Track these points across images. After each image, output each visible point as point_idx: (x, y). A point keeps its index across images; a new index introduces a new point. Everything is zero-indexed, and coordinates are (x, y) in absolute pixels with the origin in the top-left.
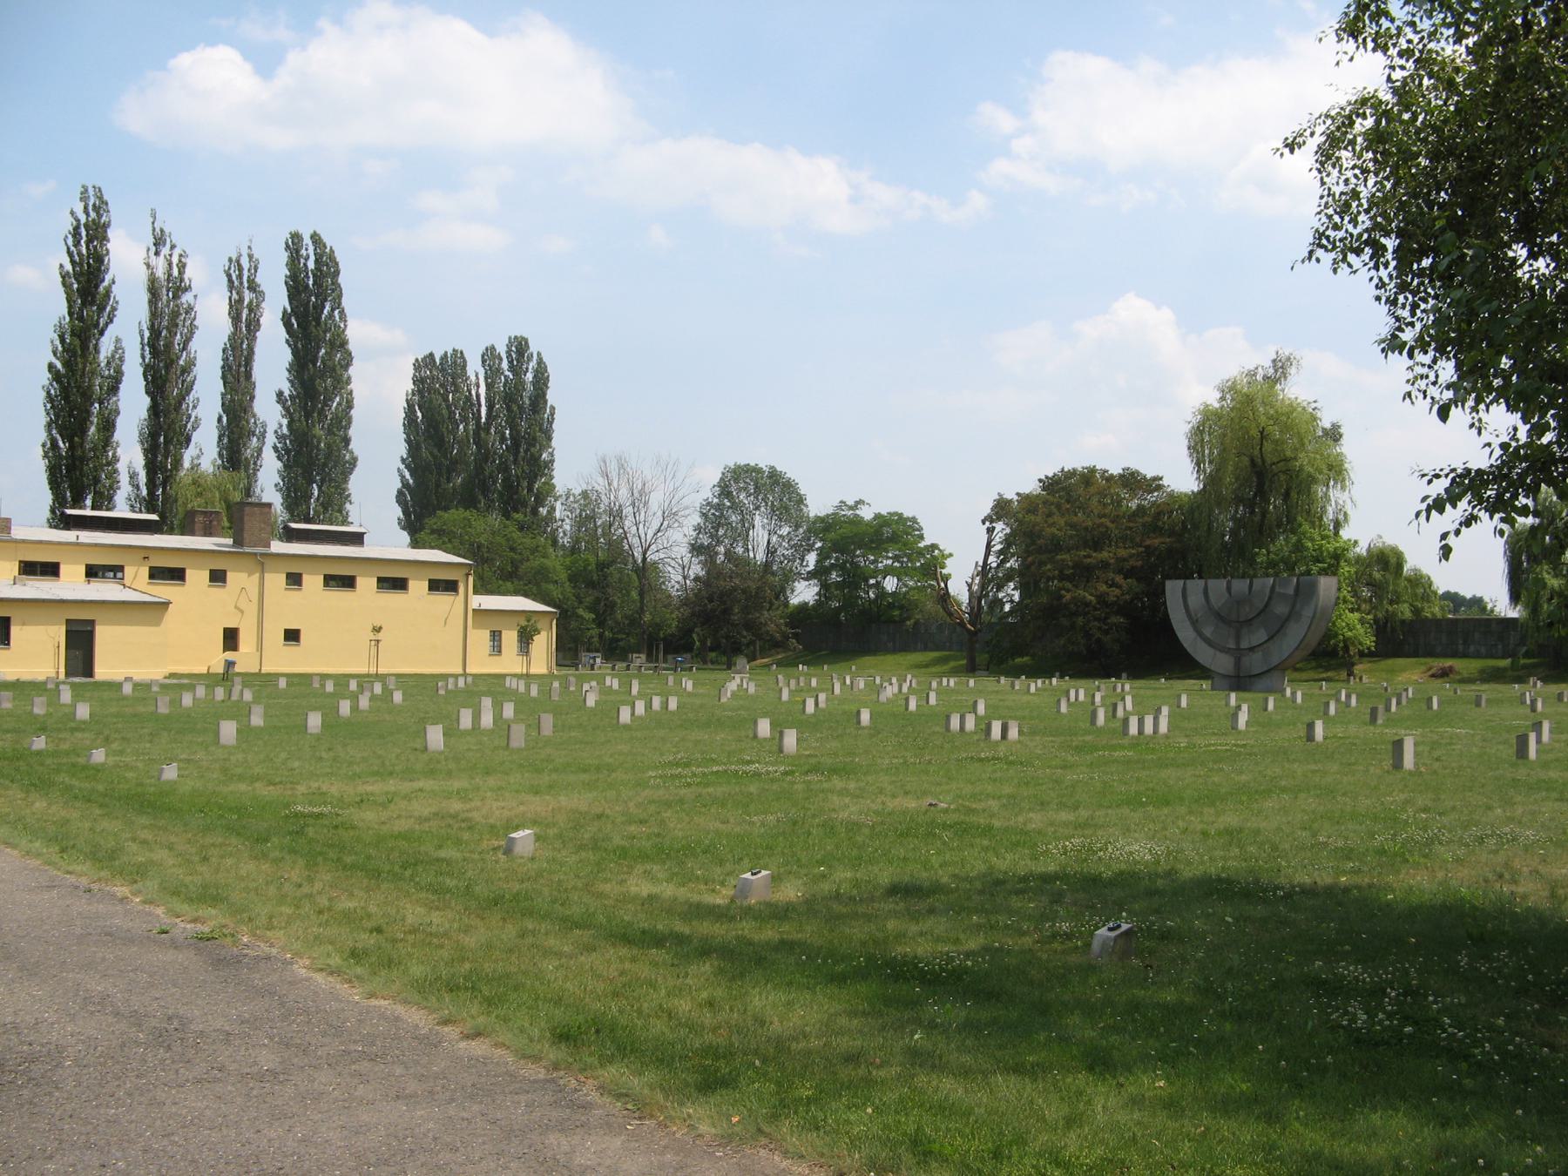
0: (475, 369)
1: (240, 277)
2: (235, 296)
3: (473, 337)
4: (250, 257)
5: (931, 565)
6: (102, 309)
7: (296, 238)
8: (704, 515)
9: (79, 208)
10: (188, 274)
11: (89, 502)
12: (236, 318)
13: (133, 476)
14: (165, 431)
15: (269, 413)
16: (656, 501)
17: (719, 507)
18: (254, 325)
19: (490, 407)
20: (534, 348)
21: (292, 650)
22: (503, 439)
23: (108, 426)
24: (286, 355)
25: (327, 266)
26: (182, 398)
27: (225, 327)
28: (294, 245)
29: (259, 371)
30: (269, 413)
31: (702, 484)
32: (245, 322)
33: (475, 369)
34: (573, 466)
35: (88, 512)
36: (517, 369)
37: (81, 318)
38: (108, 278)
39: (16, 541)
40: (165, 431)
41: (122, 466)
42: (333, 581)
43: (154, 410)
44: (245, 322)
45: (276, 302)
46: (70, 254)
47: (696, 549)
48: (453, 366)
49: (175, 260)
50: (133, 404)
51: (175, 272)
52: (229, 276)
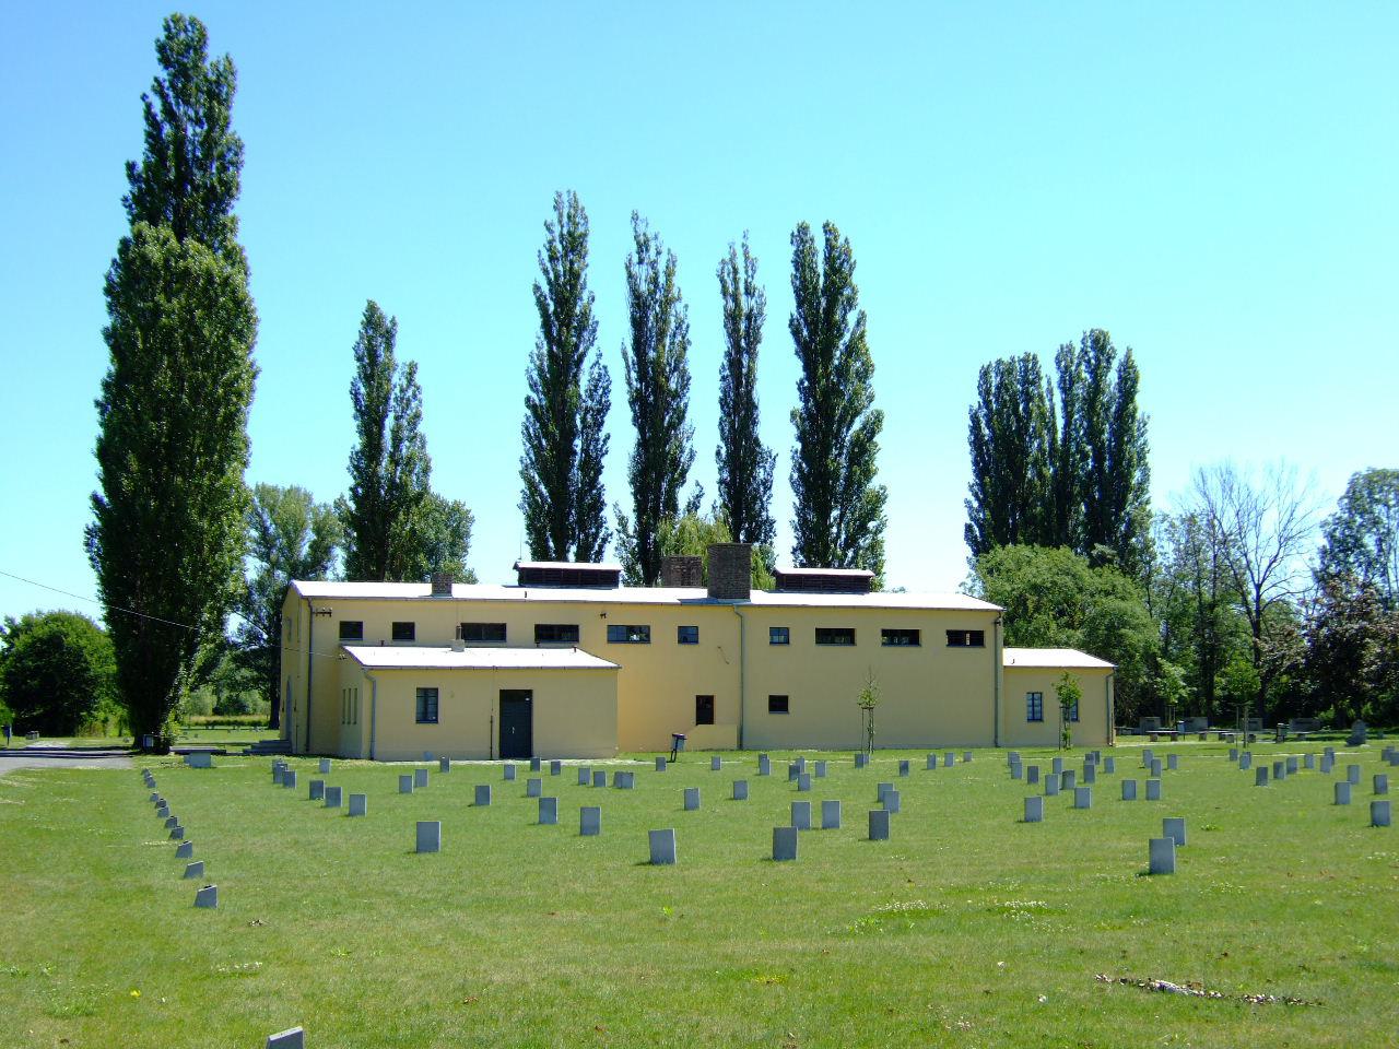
0: (1049, 372)
1: (735, 280)
2: (731, 304)
3: (1043, 337)
4: (746, 253)
5: (868, 479)
6: (581, 329)
7: (803, 229)
8: (1331, 536)
9: (553, 217)
10: (676, 281)
11: (571, 556)
12: (733, 333)
13: (622, 521)
14: (657, 469)
15: (778, 434)
16: (1270, 525)
17: (1348, 524)
18: (753, 337)
19: (1068, 417)
20: (1118, 345)
21: (778, 717)
22: (1085, 457)
23: (593, 467)
24: (796, 369)
25: (839, 265)
26: (674, 426)
27: (625, 333)
28: (801, 236)
29: (762, 393)
30: (778, 434)
31: (1324, 502)
32: (743, 334)
33: (1049, 372)
34: (1170, 489)
35: (572, 564)
36: (1097, 374)
37: (560, 344)
38: (585, 295)
39: (457, 600)
40: (657, 469)
41: (608, 514)
42: (826, 636)
43: (643, 444)
44: (743, 334)
45: (779, 308)
46: (546, 272)
47: (1322, 578)
48: (1028, 369)
49: (661, 267)
50: (621, 436)
51: (662, 280)
52: (722, 281)
